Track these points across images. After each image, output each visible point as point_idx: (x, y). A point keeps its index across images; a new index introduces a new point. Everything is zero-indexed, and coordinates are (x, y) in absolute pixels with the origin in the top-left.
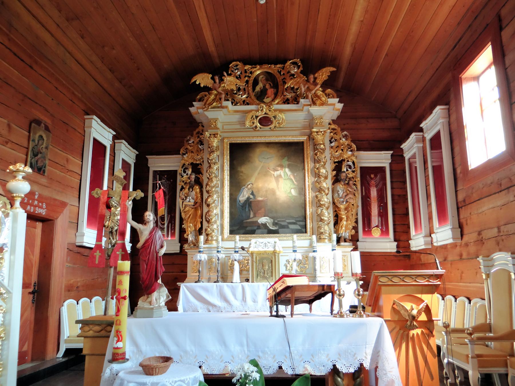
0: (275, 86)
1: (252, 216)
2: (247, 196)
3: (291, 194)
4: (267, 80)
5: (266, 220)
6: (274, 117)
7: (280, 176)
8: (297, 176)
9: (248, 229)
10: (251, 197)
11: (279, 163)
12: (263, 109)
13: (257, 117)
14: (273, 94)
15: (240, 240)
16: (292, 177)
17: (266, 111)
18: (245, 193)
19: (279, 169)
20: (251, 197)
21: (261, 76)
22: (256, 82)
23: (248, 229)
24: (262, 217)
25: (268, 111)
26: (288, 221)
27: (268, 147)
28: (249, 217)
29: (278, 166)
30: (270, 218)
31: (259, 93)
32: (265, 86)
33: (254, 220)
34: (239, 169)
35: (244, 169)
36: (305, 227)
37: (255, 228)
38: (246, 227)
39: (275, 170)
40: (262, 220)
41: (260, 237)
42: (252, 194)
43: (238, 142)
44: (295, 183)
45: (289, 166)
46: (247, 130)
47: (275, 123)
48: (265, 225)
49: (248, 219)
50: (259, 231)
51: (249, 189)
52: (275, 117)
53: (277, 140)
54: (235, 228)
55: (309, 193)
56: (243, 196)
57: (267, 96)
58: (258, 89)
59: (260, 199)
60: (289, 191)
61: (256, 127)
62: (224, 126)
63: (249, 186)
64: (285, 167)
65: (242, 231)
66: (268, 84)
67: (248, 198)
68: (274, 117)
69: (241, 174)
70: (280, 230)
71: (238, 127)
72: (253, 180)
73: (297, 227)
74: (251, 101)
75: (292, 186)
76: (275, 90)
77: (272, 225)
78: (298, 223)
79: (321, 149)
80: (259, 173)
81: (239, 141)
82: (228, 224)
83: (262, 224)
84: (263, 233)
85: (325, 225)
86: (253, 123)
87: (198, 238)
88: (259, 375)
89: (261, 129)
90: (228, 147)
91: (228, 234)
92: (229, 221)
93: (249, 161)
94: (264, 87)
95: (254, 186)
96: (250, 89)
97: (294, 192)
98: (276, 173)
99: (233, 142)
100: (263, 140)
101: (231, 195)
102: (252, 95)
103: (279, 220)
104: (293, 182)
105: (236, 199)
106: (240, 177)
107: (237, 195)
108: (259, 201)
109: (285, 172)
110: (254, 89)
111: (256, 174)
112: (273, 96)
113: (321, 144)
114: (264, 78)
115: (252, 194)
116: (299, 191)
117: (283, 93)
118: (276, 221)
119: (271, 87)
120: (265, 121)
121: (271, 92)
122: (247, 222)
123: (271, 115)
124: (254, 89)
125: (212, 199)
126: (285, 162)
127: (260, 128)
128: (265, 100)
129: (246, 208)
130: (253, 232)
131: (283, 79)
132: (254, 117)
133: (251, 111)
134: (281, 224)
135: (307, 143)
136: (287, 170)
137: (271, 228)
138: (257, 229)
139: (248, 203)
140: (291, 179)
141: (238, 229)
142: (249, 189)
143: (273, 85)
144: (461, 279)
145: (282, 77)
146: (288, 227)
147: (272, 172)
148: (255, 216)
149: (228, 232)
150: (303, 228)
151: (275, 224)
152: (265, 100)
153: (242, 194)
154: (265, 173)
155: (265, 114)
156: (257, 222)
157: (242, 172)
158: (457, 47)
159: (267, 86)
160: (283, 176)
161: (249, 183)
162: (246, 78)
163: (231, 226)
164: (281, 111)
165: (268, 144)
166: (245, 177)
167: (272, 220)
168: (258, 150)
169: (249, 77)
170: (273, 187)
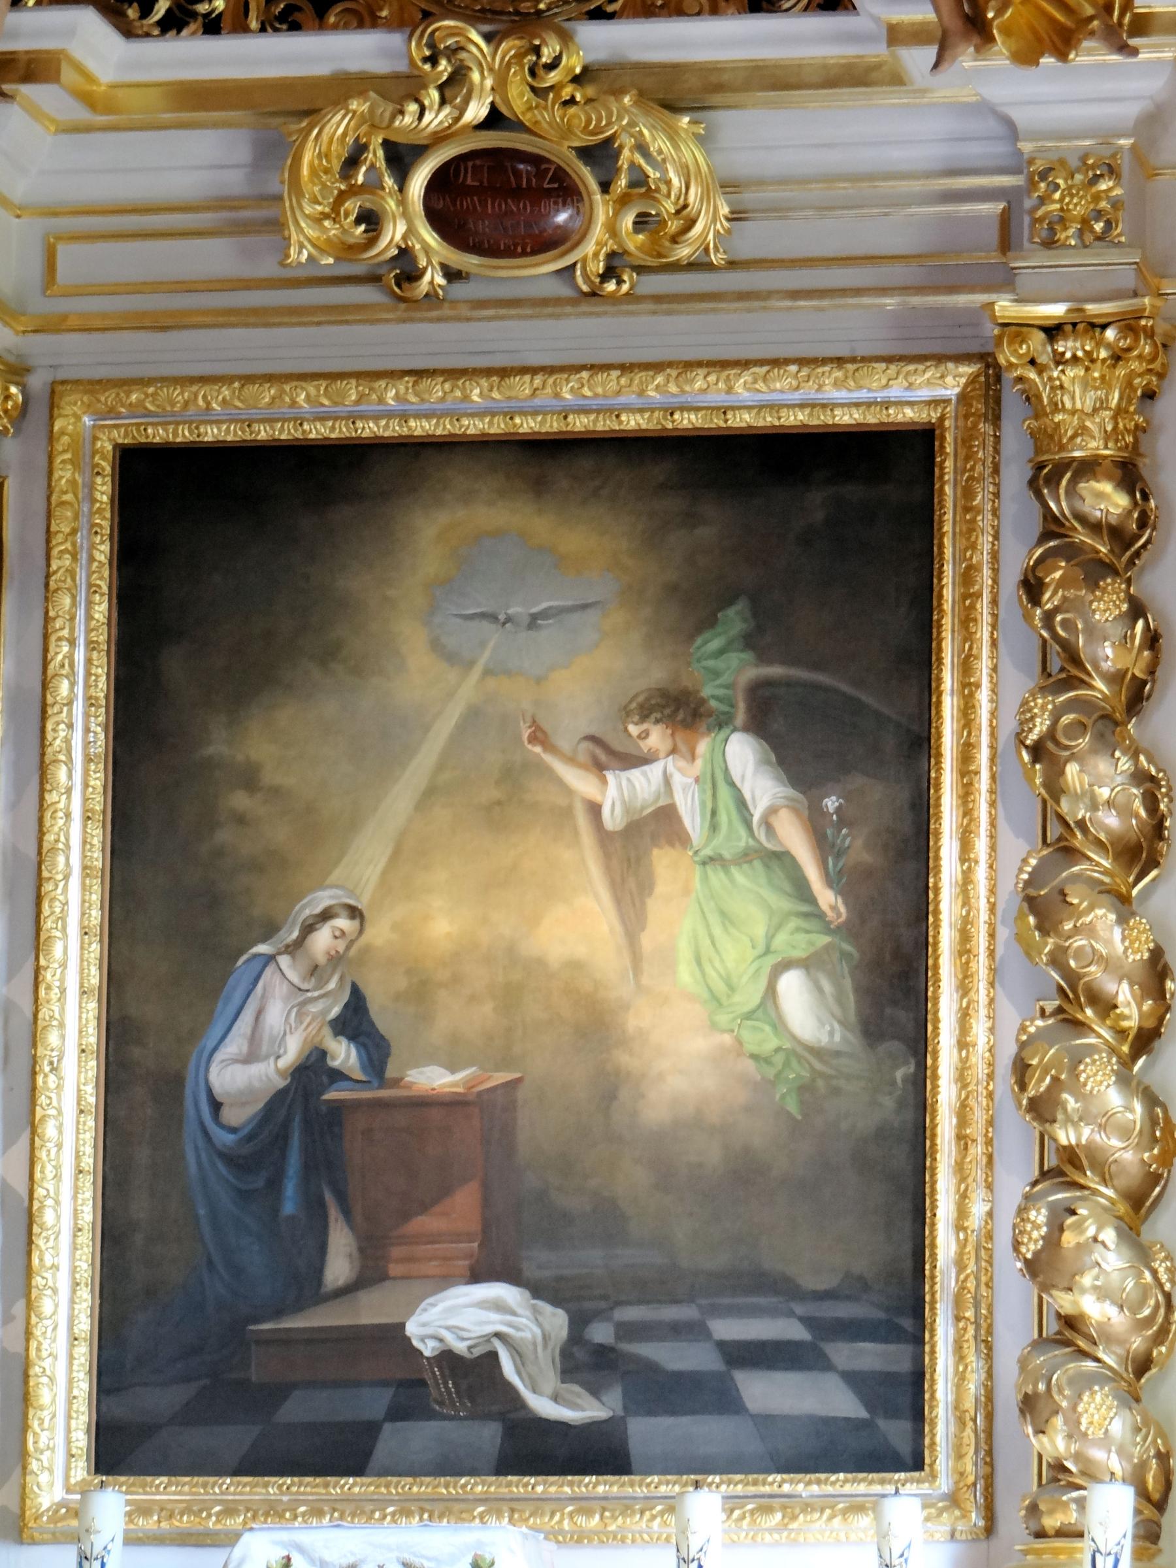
1: (339, 1267)
2: (292, 1051)
3: (779, 1024)
5: (495, 1322)
6: (585, 153)
7: (662, 823)
8: (843, 819)
9: (298, 1409)
10: (344, 1054)
11: (657, 675)
12: (458, 76)
13: (400, 159)
15: (132, 1540)
16: (794, 838)
17: (500, 86)
18: (275, 1015)
19: (656, 737)
20: (344, 1054)
23: (298, 1409)
24: (445, 1281)
25: (519, 99)
26: (728, 1329)
27: (539, 487)
28: (306, 1286)
29: (645, 713)
30: (537, 1290)
33: (369, 1310)
34: (218, 745)
35: (277, 746)
36: (908, 1394)
37: (373, 1403)
38: (278, 1393)
39: (610, 756)
40: (455, 1316)
41: (406, 1509)
42: (354, 1020)
43: (211, 434)
44: (826, 898)
45: (765, 714)
46: (290, 299)
47: (602, 226)
48: (474, 1376)
49: (298, 1307)
50: (420, 1436)
51: (314, 970)
52: (600, 154)
53: (638, 407)
54: (158, 1399)
55: (964, 1016)
56: (258, 1046)
59: (433, 1079)
60: (750, 996)
61: (406, 267)
62: (64, 251)
63: (323, 940)
64: (723, 722)
65: (238, 1437)
67: (312, 1070)
68: (585, 153)
69: (240, 800)
70: (644, 1432)
71: (216, 257)
72: (362, 867)
73: (822, 1397)
75: (797, 940)
77: (551, 1379)
78: (843, 1353)
79: (1095, 527)
80: (430, 795)
81: (217, 421)
82: (84, 1354)
83: (447, 1358)
84: (449, 1466)
85: (1083, 1383)
86: (371, 220)
89: (460, 290)
90: (104, 491)
91: (81, 1470)
92: (85, 1325)
93: (329, 655)
95: (380, 934)
97: (807, 1011)
98: (622, 793)
99: (158, 435)
100: (477, 410)
101: (120, 1035)
103: (632, 1314)
104: (802, 891)
105: (178, 1081)
106: (224, 835)
107: (195, 1035)
108: (424, 1103)
109: (719, 779)
111: (398, 803)
113: (1088, 468)
115: (354, 1020)
116: (865, 992)
118: (601, 1333)
120: (498, 197)
122: (286, 1340)
123: (556, 133)
125: (1077, 797)
126: (726, 666)
127: (452, 275)
129: (275, 1184)
130: (340, 1453)
132: (376, 155)
133: (343, 87)
134: (651, 1368)
135: (966, 441)
136: (742, 753)
137: (543, 1406)
138: (397, 1413)
139: (315, 1129)
140: (781, 859)
141: (188, 1416)
142: (314, 970)
146: (725, 1401)
147: (582, 783)
148: (370, 1275)
149: (82, 1440)
150: (893, 1413)
151: (583, 1362)
153: (244, 1024)
154: (501, 789)
155: (495, 119)
156: (392, 1337)
157: (249, 779)
160: (692, 819)
161: (323, 899)
163: (111, 1376)
164: (675, 93)
165: (543, 460)
166: (280, 834)
167: (557, 1321)
168: (433, 532)
170: (581, 951)
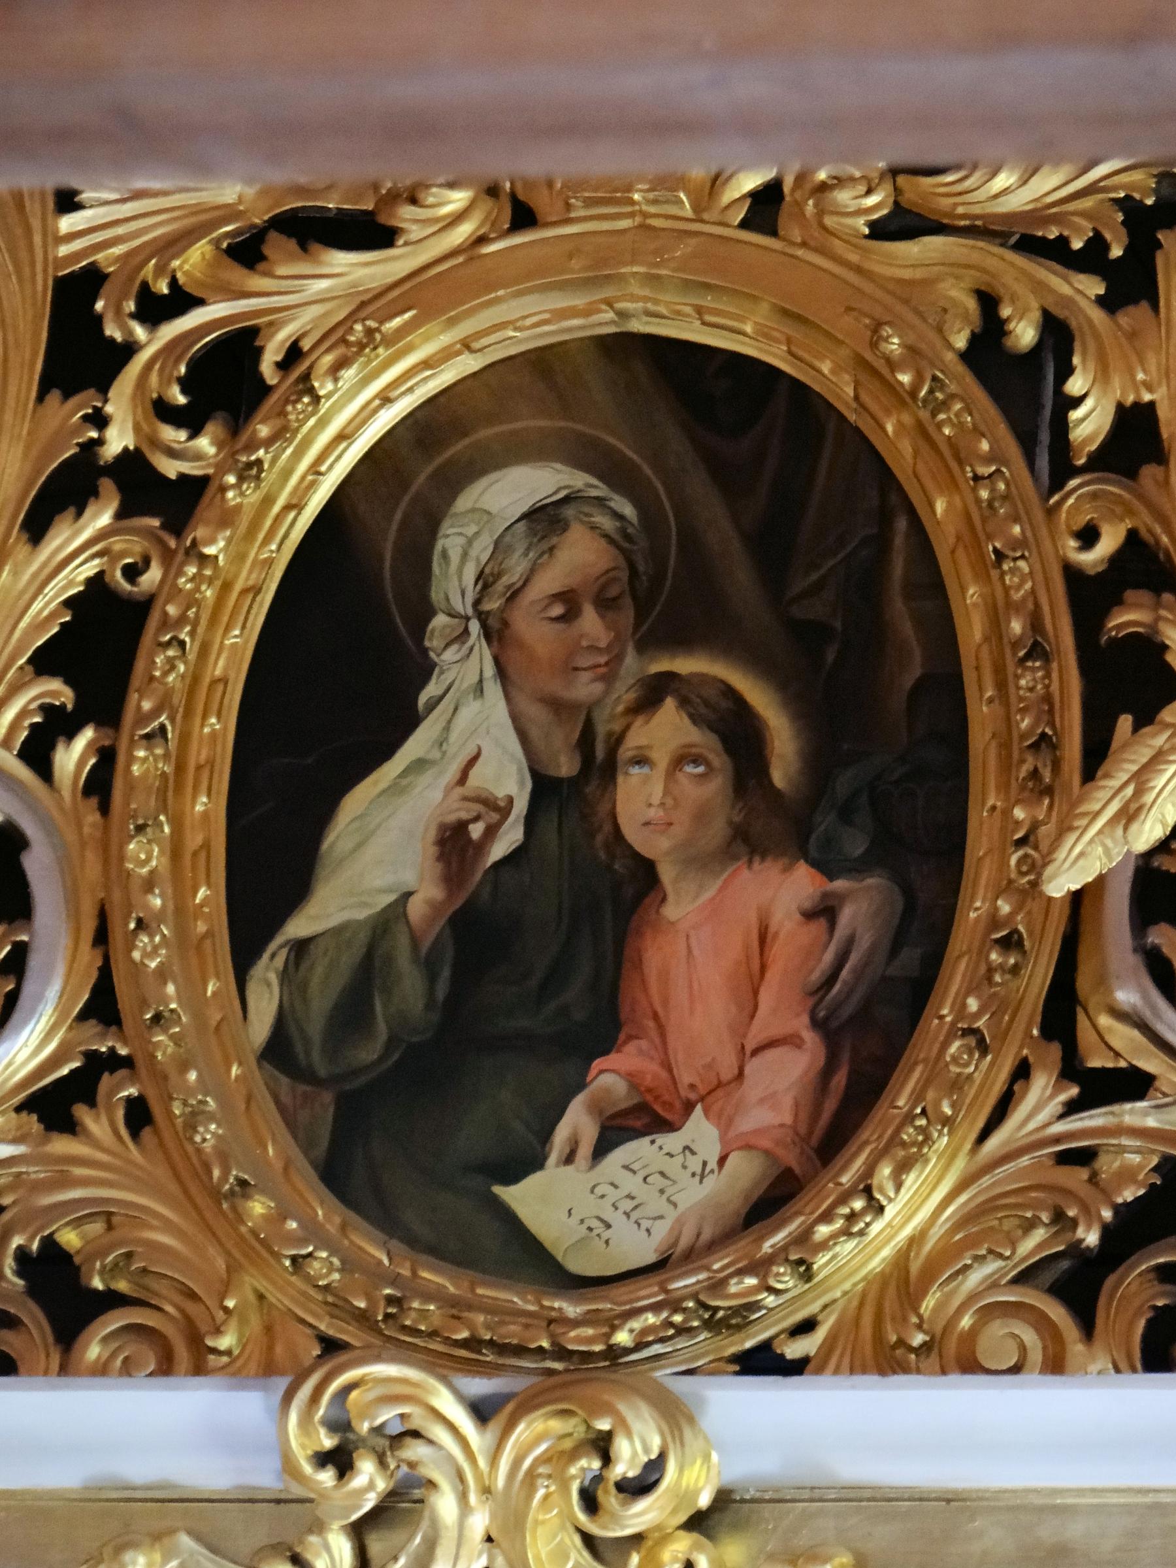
0: (884, 791)
4: (661, 597)
14: (781, 1009)
21: (511, 490)
22: (341, 661)
31: (409, 993)
32: (600, 763)
57: (609, 1078)
58: (380, 852)
66: (668, 729)
74: (164, 1230)
76: (864, 905)
87: (240, 1209)
88: (106, 1075)
94: (572, 793)
96: (174, 848)
101: (163, 1216)
102: (210, 1027)
110: (270, 861)
112: (779, 1086)
114: (580, 554)
117: (1061, 1014)
119: (763, 824)
121: (732, 942)
124: (270, 861)
128: (552, 1201)
131: (1090, 595)
143: (820, 762)
144: (92, 1558)
145: (1096, 527)
152: (552, 1201)
158: (149, 1504)
159: (659, 796)
162: (83, 547)
169: (167, 503)
